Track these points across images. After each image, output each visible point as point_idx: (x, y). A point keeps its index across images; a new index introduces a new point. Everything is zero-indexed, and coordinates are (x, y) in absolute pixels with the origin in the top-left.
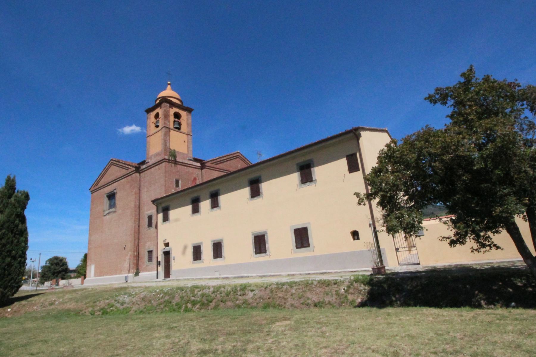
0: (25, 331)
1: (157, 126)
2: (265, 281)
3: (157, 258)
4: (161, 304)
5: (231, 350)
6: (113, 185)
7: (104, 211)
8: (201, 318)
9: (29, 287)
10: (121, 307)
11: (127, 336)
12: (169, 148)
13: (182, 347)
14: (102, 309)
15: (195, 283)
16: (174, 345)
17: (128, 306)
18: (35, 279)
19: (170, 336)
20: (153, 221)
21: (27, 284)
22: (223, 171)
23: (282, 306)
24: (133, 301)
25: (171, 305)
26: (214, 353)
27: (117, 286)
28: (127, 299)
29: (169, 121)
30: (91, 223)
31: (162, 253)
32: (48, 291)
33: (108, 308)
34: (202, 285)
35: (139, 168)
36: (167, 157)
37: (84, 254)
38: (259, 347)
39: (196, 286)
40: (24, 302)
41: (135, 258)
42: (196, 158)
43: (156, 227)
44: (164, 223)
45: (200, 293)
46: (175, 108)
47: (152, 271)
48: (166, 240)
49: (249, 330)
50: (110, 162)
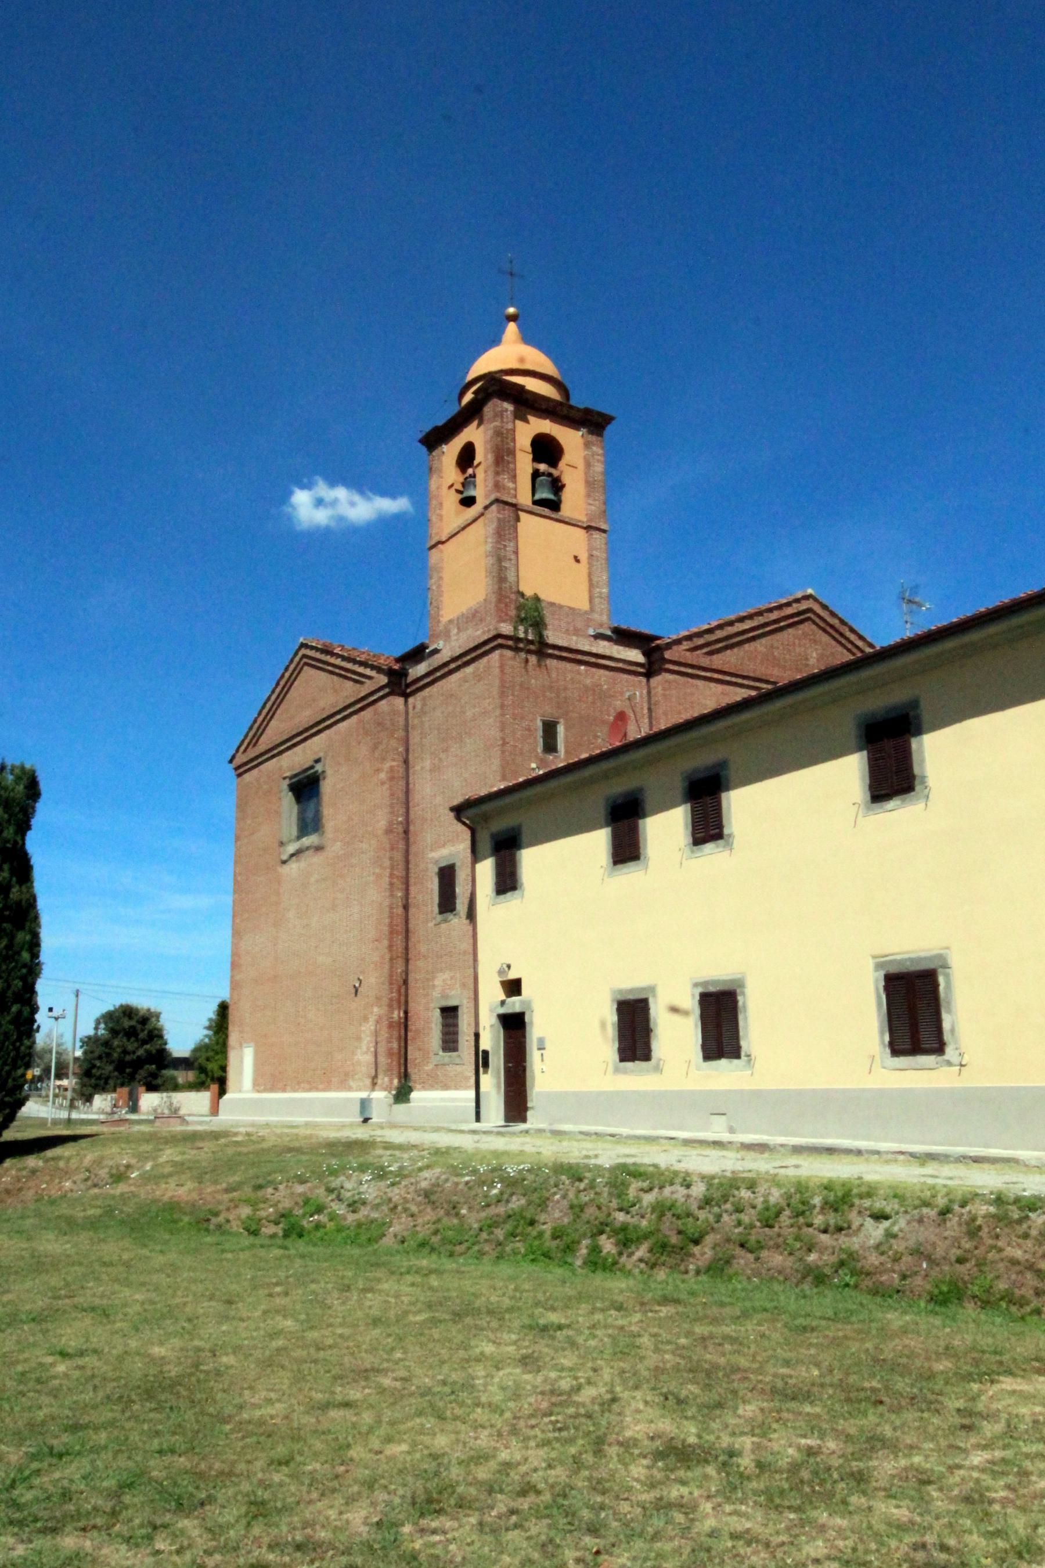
0: (39, 1265)
1: (468, 502)
2: (940, 1181)
3: (477, 1036)
4: (493, 1224)
5: (794, 1468)
6: (309, 742)
7: (282, 844)
8: (659, 1304)
9: (44, 1108)
10: (351, 1218)
11: (376, 1332)
12: (515, 589)
13: (589, 1416)
14: (283, 1216)
15: (628, 1156)
16: (554, 1399)
17: (375, 1215)
18: (65, 1082)
19: (537, 1360)
20: (457, 890)
21: (40, 1096)
22: (740, 681)
23: (1022, 1302)
24: (390, 1200)
25: (534, 1233)
26: (724, 1464)
27: (333, 1135)
28: (371, 1191)
29: (514, 478)
30: (239, 888)
31: (494, 1020)
32: (104, 1129)
33: (304, 1216)
34: (655, 1166)
35: (403, 673)
36: (506, 629)
37: (218, 1001)
38: (925, 1477)
39: (632, 1168)
40: (32, 1161)
41: (395, 1034)
42: (624, 626)
43: (471, 915)
44: (502, 897)
45: (648, 1199)
46: (534, 416)
47: (456, 1088)
48: (509, 967)
49: (874, 1390)
50: (296, 654)
